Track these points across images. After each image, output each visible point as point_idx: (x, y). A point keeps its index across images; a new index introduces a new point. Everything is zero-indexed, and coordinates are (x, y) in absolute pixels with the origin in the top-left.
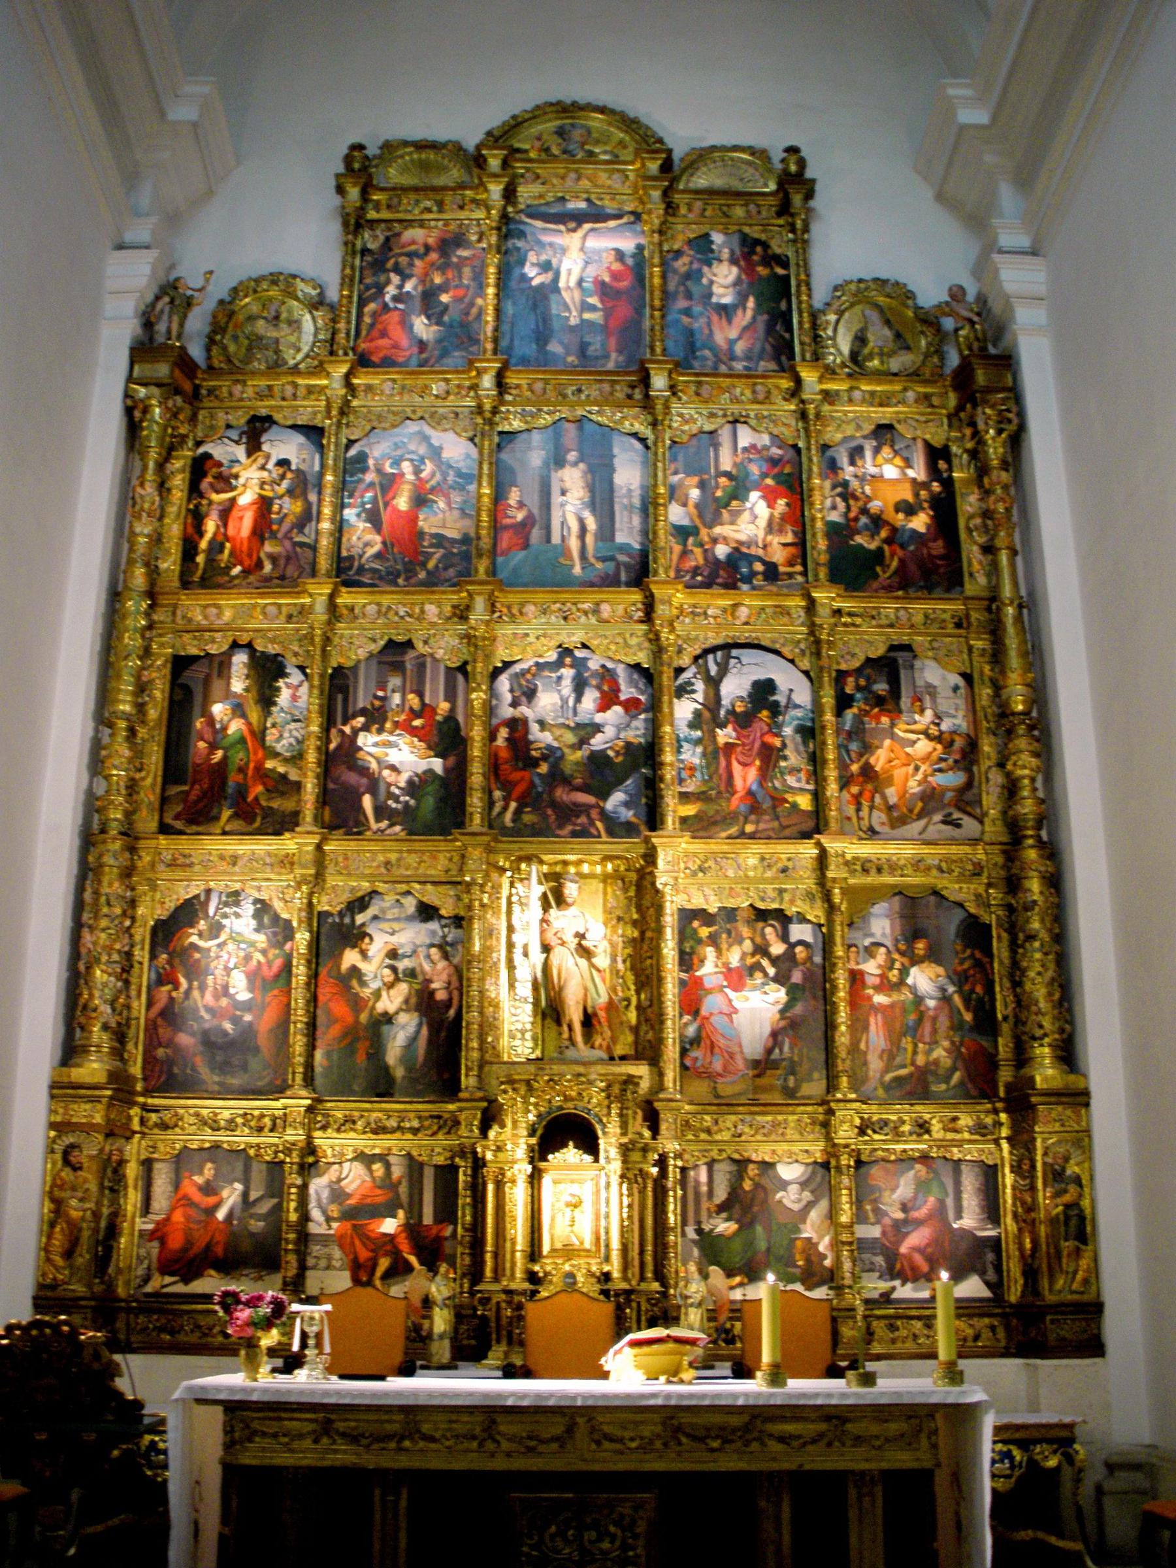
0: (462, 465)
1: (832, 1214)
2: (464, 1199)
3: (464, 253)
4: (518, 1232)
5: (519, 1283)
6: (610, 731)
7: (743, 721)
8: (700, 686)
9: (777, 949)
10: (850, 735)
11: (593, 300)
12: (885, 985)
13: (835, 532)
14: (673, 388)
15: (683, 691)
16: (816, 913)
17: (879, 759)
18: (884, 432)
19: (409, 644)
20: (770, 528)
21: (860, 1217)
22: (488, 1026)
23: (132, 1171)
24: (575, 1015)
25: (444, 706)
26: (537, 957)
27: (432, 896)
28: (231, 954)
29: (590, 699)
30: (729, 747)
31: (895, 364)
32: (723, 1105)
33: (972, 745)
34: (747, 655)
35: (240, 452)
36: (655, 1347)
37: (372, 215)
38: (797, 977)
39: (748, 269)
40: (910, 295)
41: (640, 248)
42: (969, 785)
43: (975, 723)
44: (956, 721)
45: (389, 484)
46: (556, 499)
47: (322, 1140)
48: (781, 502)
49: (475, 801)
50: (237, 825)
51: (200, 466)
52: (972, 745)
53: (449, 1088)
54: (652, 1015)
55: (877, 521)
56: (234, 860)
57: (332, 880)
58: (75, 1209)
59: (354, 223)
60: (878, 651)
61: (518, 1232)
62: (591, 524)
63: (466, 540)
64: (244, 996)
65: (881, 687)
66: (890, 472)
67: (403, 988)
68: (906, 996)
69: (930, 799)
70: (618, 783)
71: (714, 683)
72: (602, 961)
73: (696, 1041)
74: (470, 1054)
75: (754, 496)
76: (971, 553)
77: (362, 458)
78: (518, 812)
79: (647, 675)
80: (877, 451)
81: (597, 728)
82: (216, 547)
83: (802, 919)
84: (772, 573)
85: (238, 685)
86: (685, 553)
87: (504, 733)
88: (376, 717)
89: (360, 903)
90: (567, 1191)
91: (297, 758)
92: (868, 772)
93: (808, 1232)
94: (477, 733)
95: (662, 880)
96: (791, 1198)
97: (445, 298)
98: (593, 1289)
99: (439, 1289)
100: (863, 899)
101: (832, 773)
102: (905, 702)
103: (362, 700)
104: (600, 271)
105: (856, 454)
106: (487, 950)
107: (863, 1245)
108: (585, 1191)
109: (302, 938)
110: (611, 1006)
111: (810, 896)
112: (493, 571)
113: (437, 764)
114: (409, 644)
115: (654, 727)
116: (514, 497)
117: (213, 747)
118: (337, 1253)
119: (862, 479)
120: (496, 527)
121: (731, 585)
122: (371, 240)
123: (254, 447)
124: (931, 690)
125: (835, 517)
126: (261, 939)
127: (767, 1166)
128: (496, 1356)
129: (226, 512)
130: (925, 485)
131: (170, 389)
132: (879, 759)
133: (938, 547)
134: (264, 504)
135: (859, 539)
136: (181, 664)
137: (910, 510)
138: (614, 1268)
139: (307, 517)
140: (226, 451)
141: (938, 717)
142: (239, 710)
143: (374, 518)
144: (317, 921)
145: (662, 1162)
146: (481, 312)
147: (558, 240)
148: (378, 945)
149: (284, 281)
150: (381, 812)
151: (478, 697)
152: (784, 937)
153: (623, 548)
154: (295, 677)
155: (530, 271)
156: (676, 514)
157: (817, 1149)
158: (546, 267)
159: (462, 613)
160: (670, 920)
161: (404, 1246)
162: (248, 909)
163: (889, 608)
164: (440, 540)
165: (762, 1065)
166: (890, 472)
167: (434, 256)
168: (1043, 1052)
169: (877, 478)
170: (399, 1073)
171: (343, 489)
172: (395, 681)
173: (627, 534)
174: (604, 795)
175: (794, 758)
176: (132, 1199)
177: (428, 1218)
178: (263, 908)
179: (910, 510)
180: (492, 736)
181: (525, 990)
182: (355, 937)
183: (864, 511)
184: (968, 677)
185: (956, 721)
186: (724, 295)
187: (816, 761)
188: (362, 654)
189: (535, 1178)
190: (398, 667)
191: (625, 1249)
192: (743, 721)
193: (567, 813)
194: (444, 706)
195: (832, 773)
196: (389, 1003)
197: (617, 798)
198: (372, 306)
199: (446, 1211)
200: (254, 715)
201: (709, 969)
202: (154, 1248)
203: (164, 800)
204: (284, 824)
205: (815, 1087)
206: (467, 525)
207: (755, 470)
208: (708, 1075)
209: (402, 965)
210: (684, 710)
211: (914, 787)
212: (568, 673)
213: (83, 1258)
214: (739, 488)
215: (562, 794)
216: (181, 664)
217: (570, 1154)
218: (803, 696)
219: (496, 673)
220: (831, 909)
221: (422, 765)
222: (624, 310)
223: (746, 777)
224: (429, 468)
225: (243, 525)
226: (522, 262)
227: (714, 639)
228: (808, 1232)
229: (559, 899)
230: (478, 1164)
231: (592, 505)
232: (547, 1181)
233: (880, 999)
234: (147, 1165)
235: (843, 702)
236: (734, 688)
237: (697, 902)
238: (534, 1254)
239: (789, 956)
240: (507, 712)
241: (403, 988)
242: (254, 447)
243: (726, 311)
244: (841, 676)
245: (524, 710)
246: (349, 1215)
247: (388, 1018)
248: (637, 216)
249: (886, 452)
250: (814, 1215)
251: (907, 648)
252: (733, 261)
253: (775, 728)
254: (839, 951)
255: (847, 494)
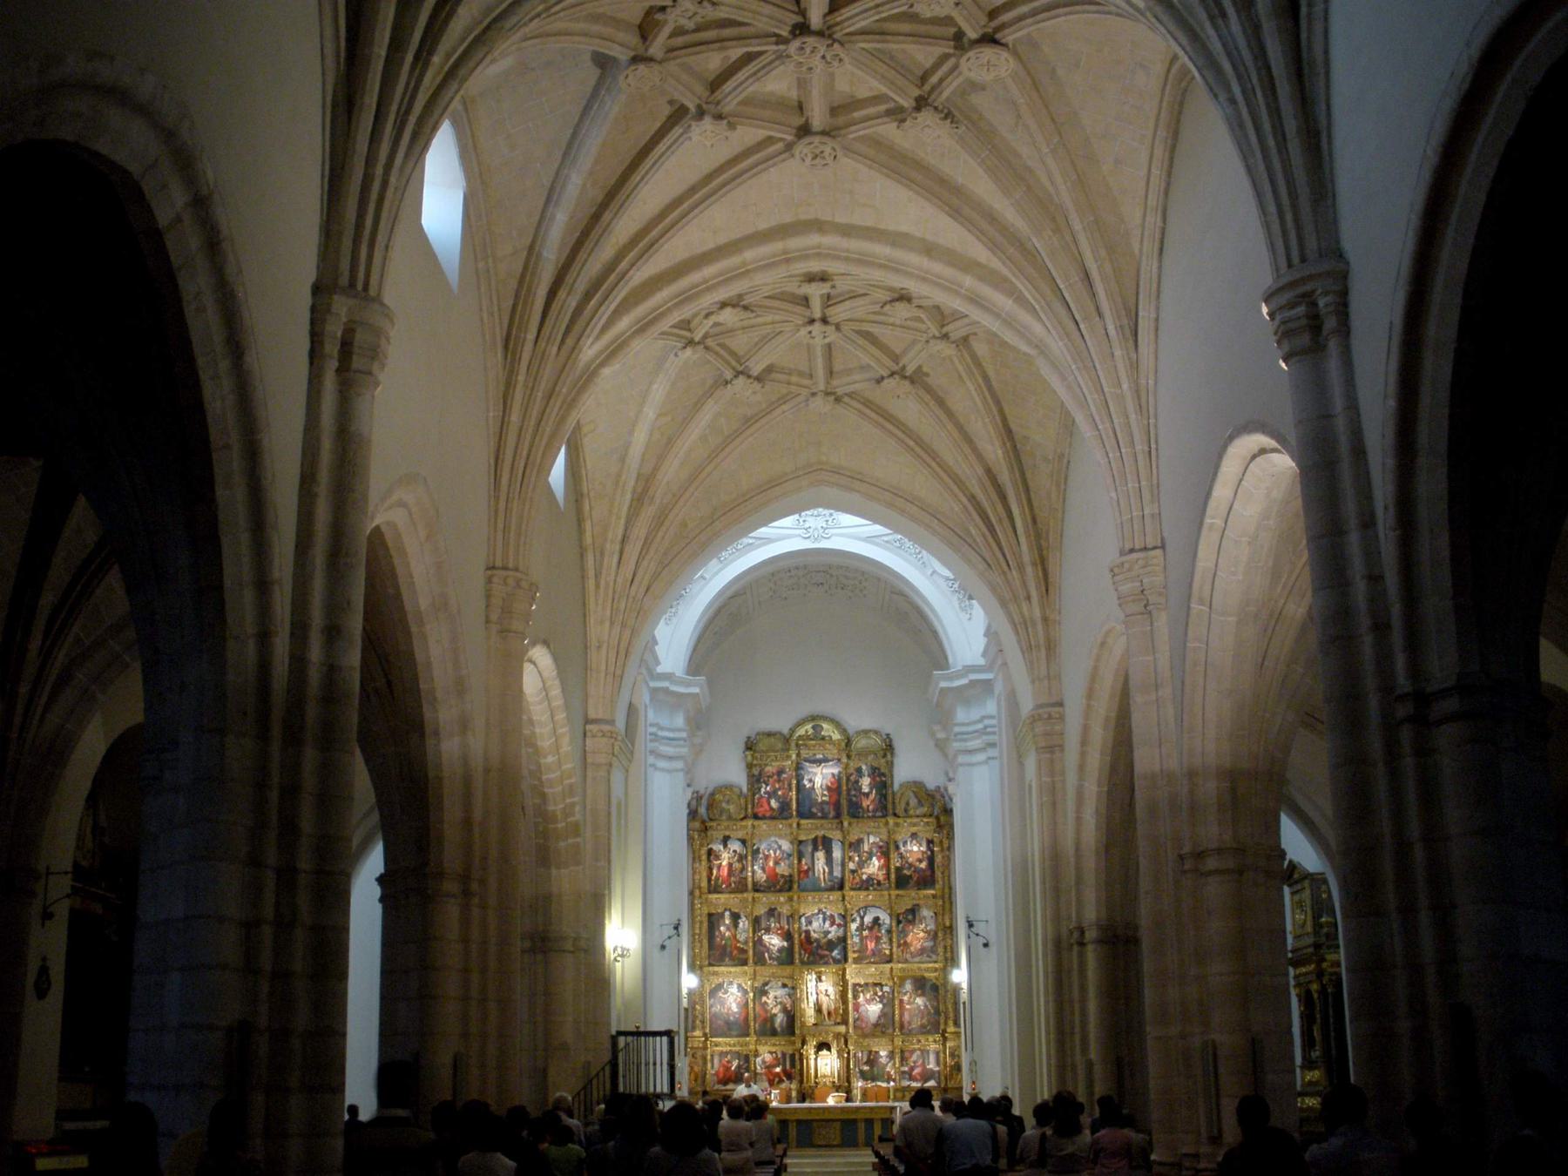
0: (789, 851)
1: (894, 1064)
2: (798, 1063)
3: (784, 776)
4: (812, 1071)
5: (813, 1084)
6: (833, 933)
7: (871, 929)
8: (858, 919)
9: (880, 994)
10: (901, 932)
11: (825, 793)
12: (909, 1003)
13: (898, 870)
14: (850, 824)
15: (854, 920)
16: (891, 983)
17: (909, 939)
18: (914, 836)
19: (776, 909)
20: (879, 869)
21: (902, 1065)
22: (803, 1015)
23: (709, 1057)
24: (825, 1012)
25: (786, 927)
26: (815, 996)
27: (786, 981)
28: (731, 999)
29: (828, 923)
30: (867, 937)
31: (918, 812)
32: (865, 1036)
33: (936, 934)
34: (872, 910)
35: (721, 847)
36: (1008, 1025)
37: (755, 762)
38: (885, 1001)
39: (873, 779)
40: (924, 786)
41: (840, 773)
42: (935, 945)
43: (937, 927)
44: (931, 927)
45: (767, 857)
46: (816, 862)
47: (758, 1047)
48: (882, 861)
49: (797, 956)
50: (730, 963)
51: (710, 852)
52: (936, 934)
53: (793, 1033)
54: (846, 1011)
55: (911, 865)
56: (730, 972)
57: (758, 978)
58: (696, 1069)
59: (750, 766)
60: (909, 907)
61: (812, 1071)
62: (827, 870)
63: (791, 876)
64: (736, 1010)
65: (910, 917)
66: (915, 848)
67: (779, 1006)
68: (915, 1006)
69: (922, 951)
70: (835, 948)
71: (862, 918)
72: (832, 997)
73: (858, 1019)
74: (798, 1024)
75: (874, 858)
76: (938, 874)
77: (758, 849)
78: (808, 958)
79: (844, 917)
80: (911, 842)
81: (829, 932)
82: (717, 878)
83: (886, 985)
84: (879, 883)
85: (727, 922)
86: (854, 878)
87: (803, 935)
88: (768, 930)
89: (766, 984)
90: (825, 1061)
91: (746, 943)
92: (905, 942)
93: (888, 1069)
94: (796, 936)
95: (848, 977)
96: (883, 1060)
97: (780, 793)
98: (831, 1085)
99: (793, 1086)
100: (902, 980)
101: (895, 945)
102: (917, 921)
103: (763, 926)
104: (827, 782)
105: (905, 843)
106: (801, 995)
107: (904, 1072)
108: (828, 1061)
109: (751, 995)
110: (835, 1009)
111: (889, 979)
112: (799, 887)
113: (785, 944)
114: (776, 909)
115: (845, 932)
116: (804, 862)
117: (722, 940)
118: (764, 1077)
119: (906, 851)
120: (800, 872)
121: (867, 889)
122: (756, 771)
123: (725, 846)
124: (925, 918)
125: (898, 865)
126: (739, 994)
127: (877, 1052)
128: (808, 1100)
129: (719, 866)
130: (925, 853)
131: (700, 831)
132: (909, 939)
133: (928, 873)
134: (730, 865)
135: (905, 872)
136: (710, 915)
137: (920, 861)
138: (836, 1080)
139: (743, 869)
140: (717, 847)
141: (926, 925)
142: (728, 929)
143: (763, 869)
144: (754, 990)
145: (848, 1053)
146: (791, 799)
147: (814, 770)
148: (771, 995)
149: (729, 787)
150: (770, 958)
151: (796, 926)
152: (882, 990)
153: (836, 877)
154: (744, 919)
155: (806, 782)
156: (852, 866)
157: (890, 1048)
158: (810, 781)
159: (791, 899)
160: (850, 987)
161: (782, 1075)
162: (735, 986)
163: (913, 893)
164: (783, 876)
165: (876, 1025)
166: (915, 848)
167: (775, 777)
168: (951, 1023)
169: (912, 851)
170: (779, 1029)
171: (754, 859)
172: (772, 919)
173: (837, 873)
174: (832, 951)
175: (885, 939)
176: (709, 1065)
177: (788, 1067)
178: (739, 986)
179: (920, 861)
180: (800, 935)
181: (812, 1005)
182: (765, 993)
183: (907, 862)
184: (935, 913)
185: (931, 927)
186: (866, 789)
187: (891, 940)
188: (762, 912)
189: (816, 1059)
190: (773, 916)
191: (839, 1076)
192: (871, 929)
193: (822, 957)
194: (786, 927)
195: (895, 945)
196: (775, 1011)
197: (835, 953)
198: (757, 796)
199: (793, 1065)
200: (733, 931)
201: (861, 999)
202: (715, 1078)
203: (709, 956)
204: (744, 963)
205: (890, 1031)
206: (790, 870)
207: (874, 850)
208: (862, 1029)
209: (779, 1000)
210: (854, 926)
211: (919, 946)
212: (821, 916)
213: (699, 1081)
214: (870, 855)
215: (820, 951)
216: (710, 915)
217: (825, 1052)
218: (888, 921)
219: (800, 917)
220: (894, 983)
221: (781, 945)
222: (835, 797)
223: (871, 945)
224: (778, 852)
225: (725, 872)
226: (803, 779)
227: (862, 905)
228: (888, 1069)
229: (821, 980)
230: (801, 1055)
231: (827, 864)
232: (819, 1059)
233: (908, 1007)
234: (712, 1056)
235: (899, 922)
236: (868, 919)
237: (857, 981)
238: (816, 1076)
239: (883, 996)
240: (804, 928)
241: (779, 1006)
242: (725, 846)
243: (867, 795)
244: (898, 915)
245: (809, 928)
246: (767, 1067)
247: (775, 1015)
248: (839, 760)
249: (914, 842)
250: (890, 1064)
251: (918, 905)
252: (869, 776)
253: (879, 931)
254: (896, 994)
255: (902, 856)
